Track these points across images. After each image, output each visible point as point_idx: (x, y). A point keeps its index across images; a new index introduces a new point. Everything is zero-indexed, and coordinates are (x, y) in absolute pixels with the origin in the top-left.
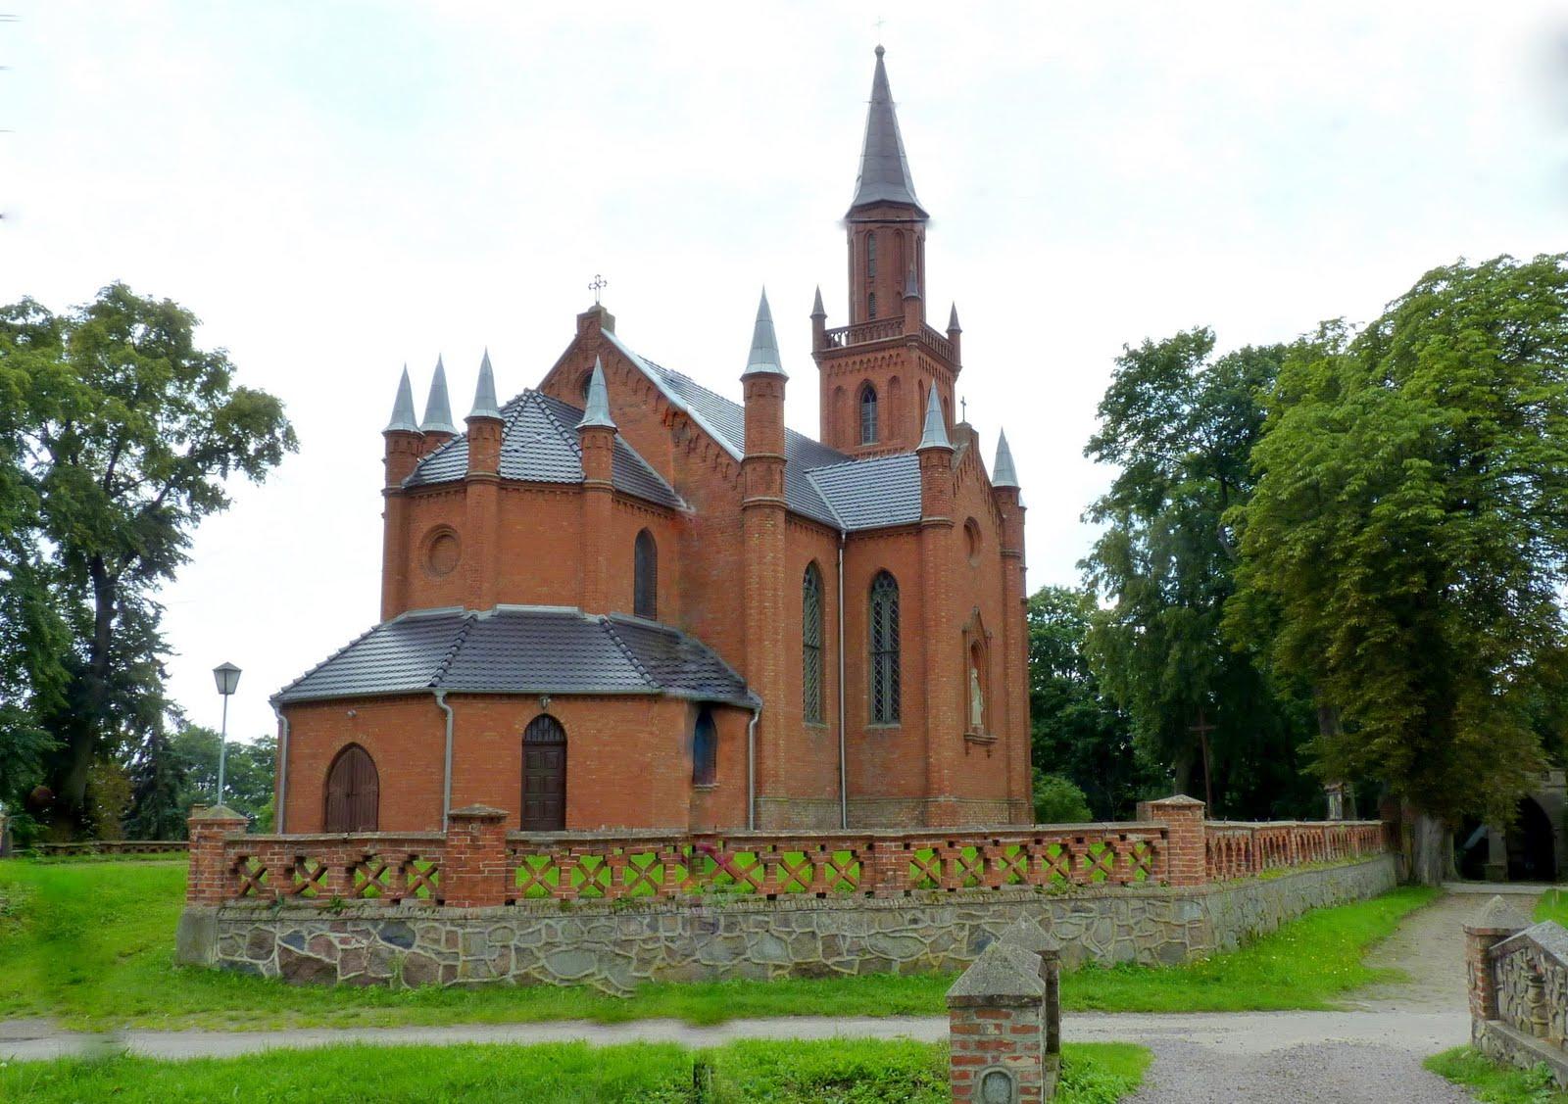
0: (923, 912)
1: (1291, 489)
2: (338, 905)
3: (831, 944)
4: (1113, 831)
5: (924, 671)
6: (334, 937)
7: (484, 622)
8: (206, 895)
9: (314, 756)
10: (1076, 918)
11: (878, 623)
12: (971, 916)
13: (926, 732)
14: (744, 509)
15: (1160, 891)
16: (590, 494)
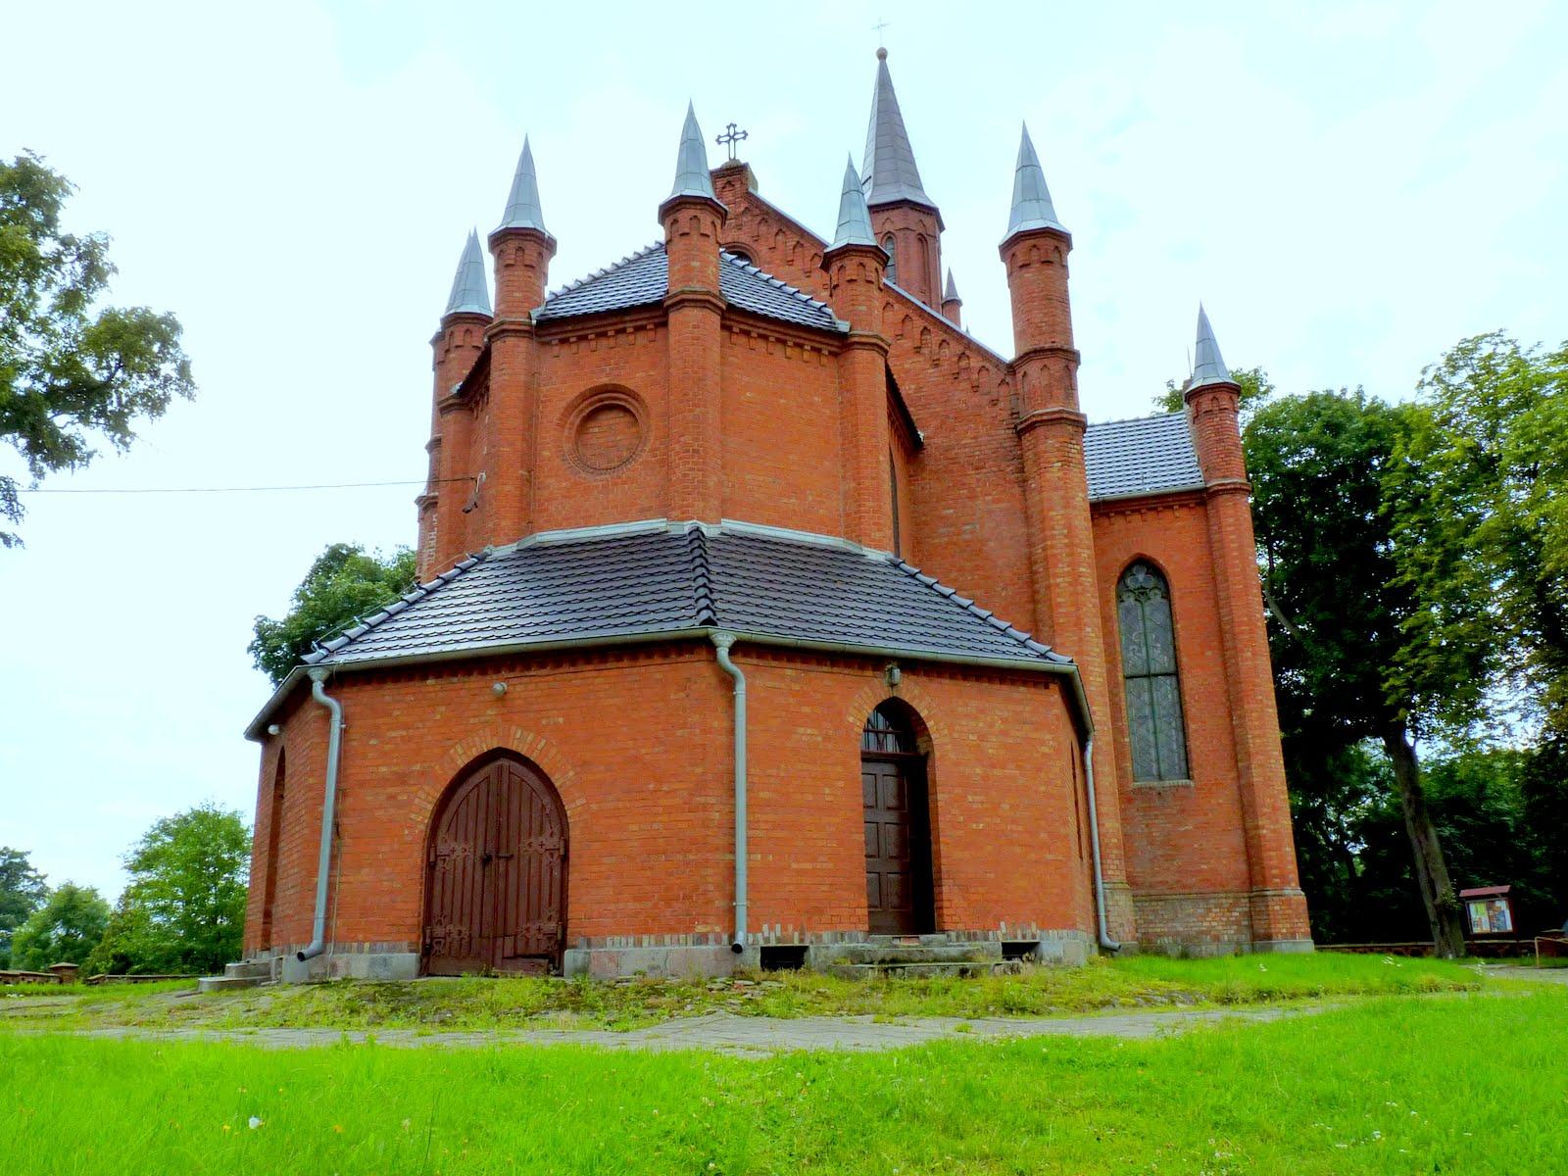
9: (402, 779)
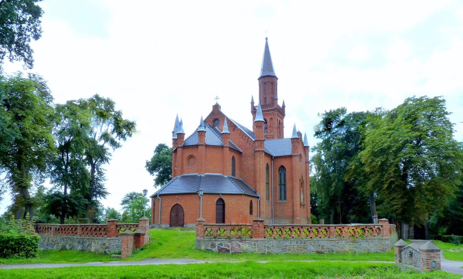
2: (229, 238)
3: (323, 247)
4: (373, 226)
5: (293, 189)
8: (200, 235)
9: (167, 206)
10: (366, 243)
13: (293, 203)
14: (255, 152)
15: (382, 238)
16: (225, 148)
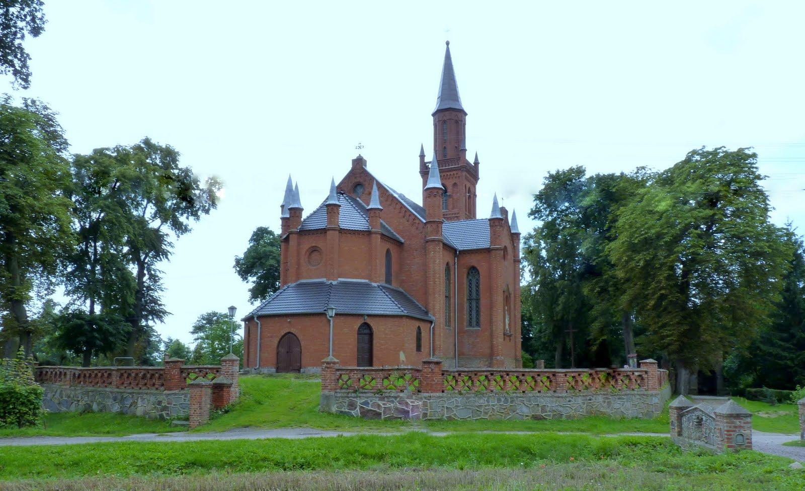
0: (593, 396)
1: (639, 239)
3: (543, 409)
5: (491, 306)
6: (381, 403)
7: (335, 285)
8: (329, 388)
9: (271, 337)
11: (470, 287)
12: (607, 398)
14: (427, 242)
